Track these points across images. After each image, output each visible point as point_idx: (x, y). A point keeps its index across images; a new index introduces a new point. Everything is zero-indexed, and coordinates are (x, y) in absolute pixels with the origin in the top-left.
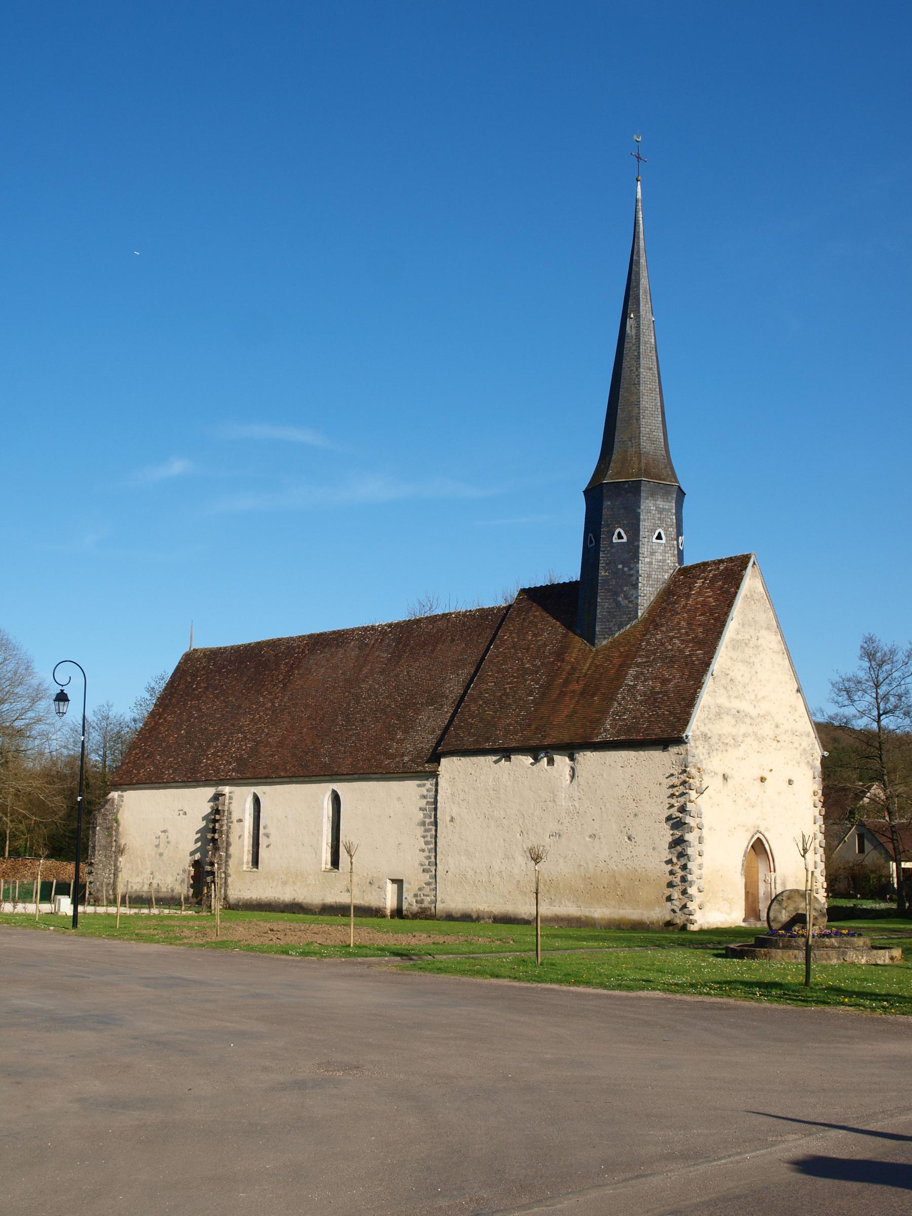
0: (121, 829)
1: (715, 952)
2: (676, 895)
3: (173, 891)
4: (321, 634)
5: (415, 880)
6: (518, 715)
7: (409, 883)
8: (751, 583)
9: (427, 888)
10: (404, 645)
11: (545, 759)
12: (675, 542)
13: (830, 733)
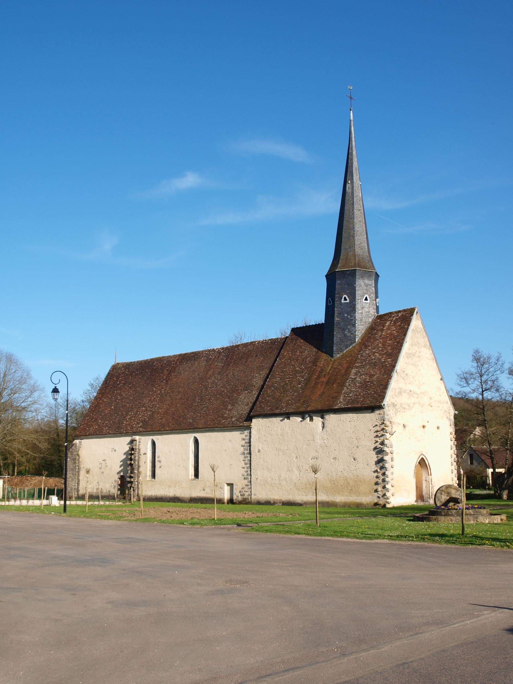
0: (80, 459)
1: (408, 518)
2: (380, 489)
3: (109, 492)
4: (186, 354)
5: (240, 484)
6: (293, 395)
7: (237, 485)
8: (416, 323)
9: (247, 488)
10: (231, 359)
11: (308, 418)
12: (375, 302)
13: (457, 402)
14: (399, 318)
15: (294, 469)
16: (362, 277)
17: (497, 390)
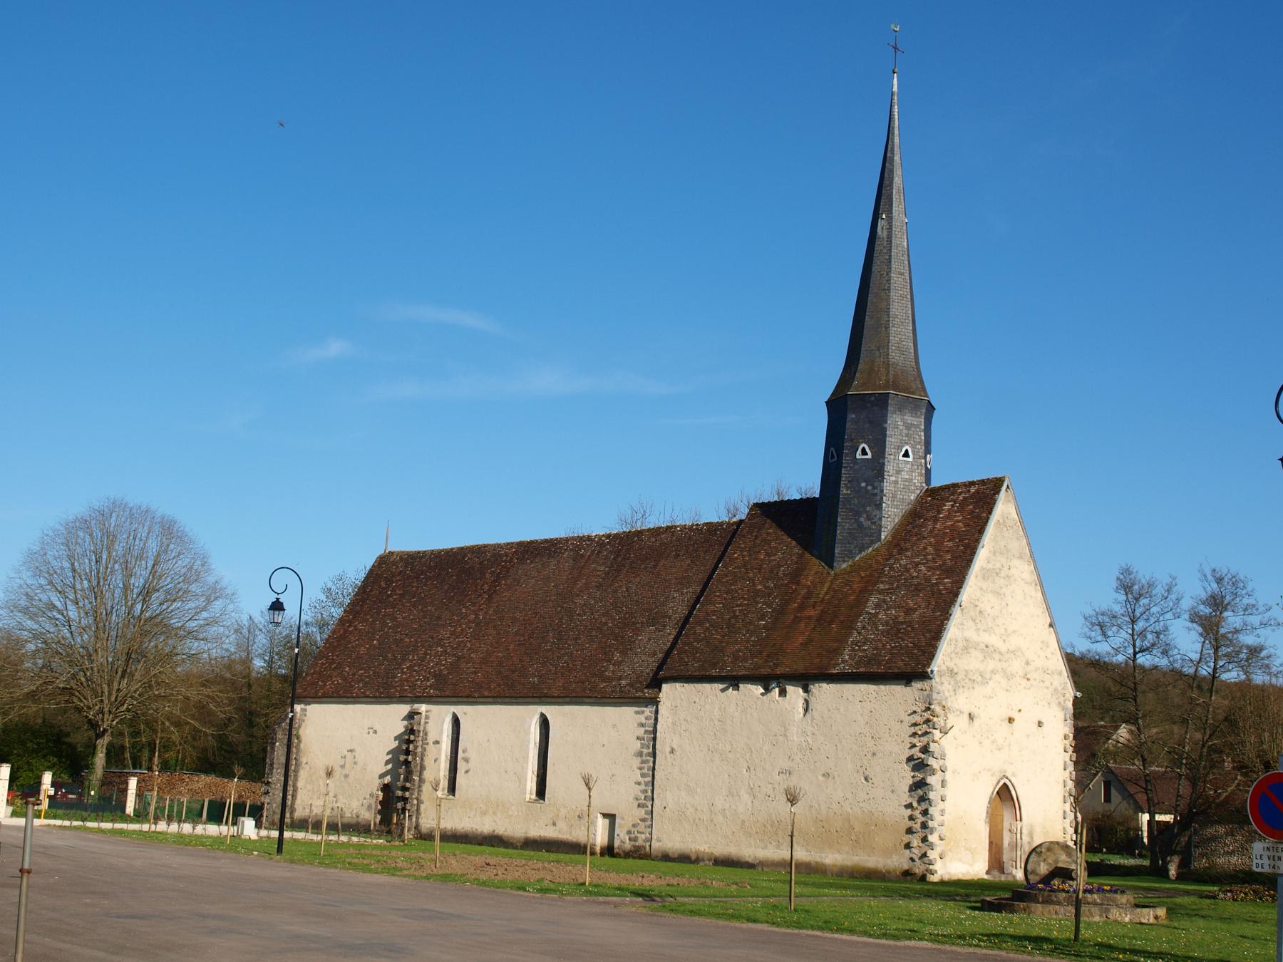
2: (915, 842)
4: (532, 542)
5: (629, 816)
6: (748, 641)
7: (623, 819)
8: (1004, 508)
9: (642, 824)
13: (1079, 667)
14: (971, 497)
15: (742, 792)
16: (900, 410)
17: (1165, 653)
